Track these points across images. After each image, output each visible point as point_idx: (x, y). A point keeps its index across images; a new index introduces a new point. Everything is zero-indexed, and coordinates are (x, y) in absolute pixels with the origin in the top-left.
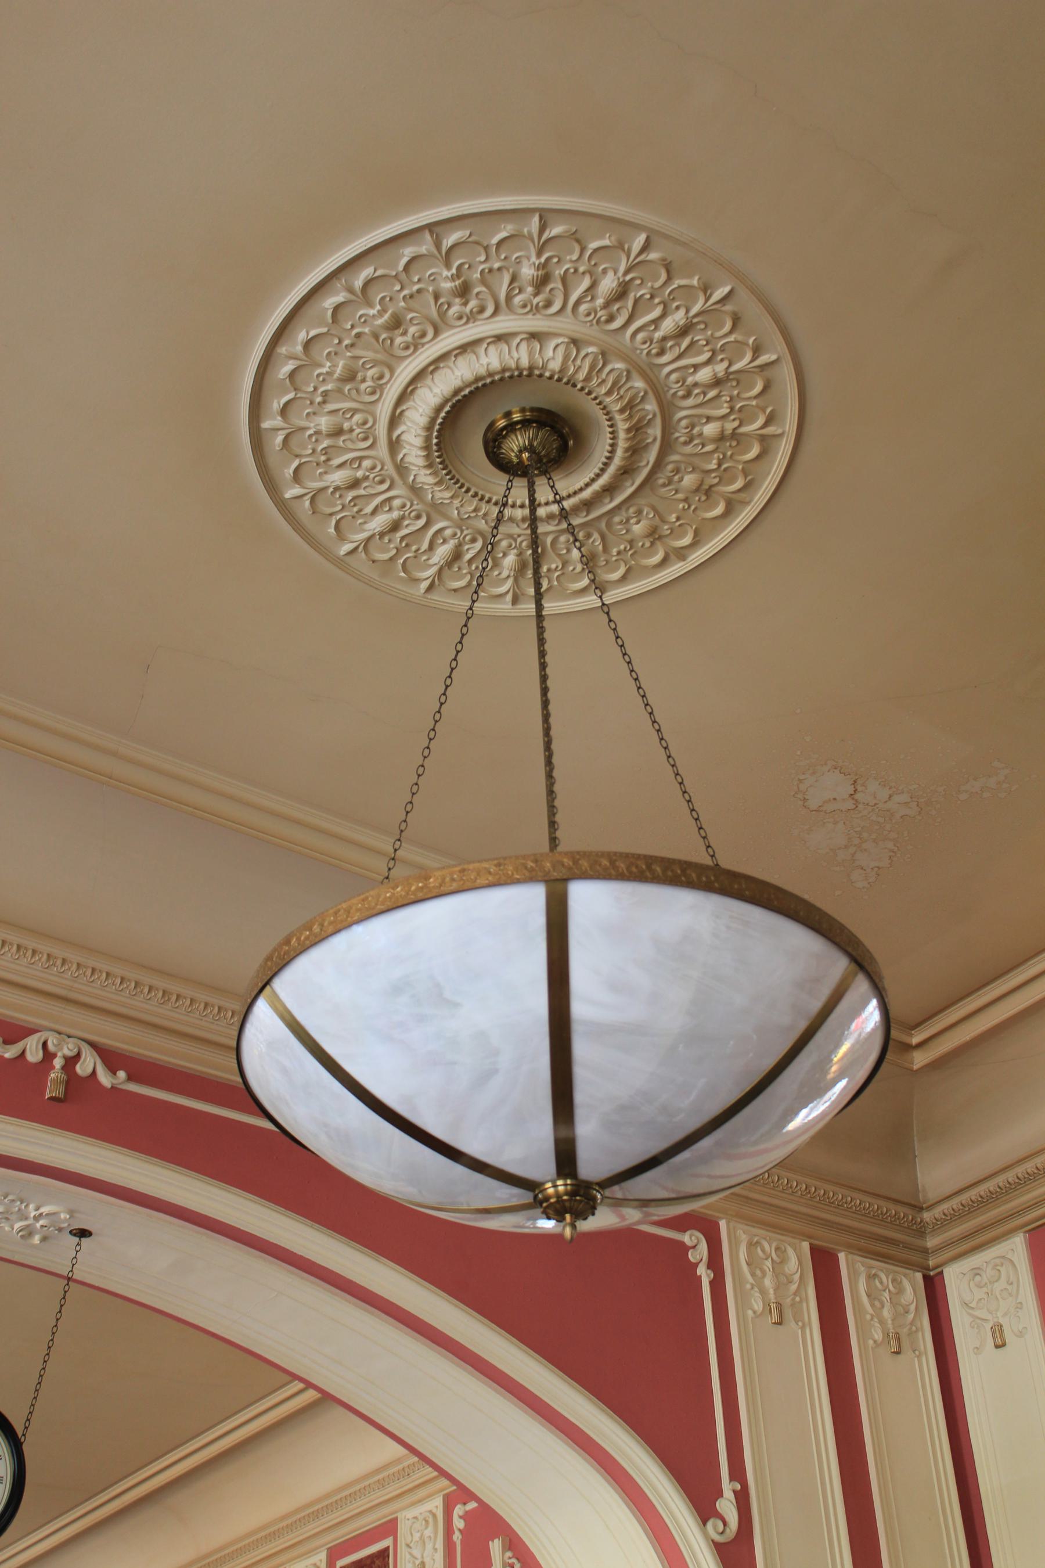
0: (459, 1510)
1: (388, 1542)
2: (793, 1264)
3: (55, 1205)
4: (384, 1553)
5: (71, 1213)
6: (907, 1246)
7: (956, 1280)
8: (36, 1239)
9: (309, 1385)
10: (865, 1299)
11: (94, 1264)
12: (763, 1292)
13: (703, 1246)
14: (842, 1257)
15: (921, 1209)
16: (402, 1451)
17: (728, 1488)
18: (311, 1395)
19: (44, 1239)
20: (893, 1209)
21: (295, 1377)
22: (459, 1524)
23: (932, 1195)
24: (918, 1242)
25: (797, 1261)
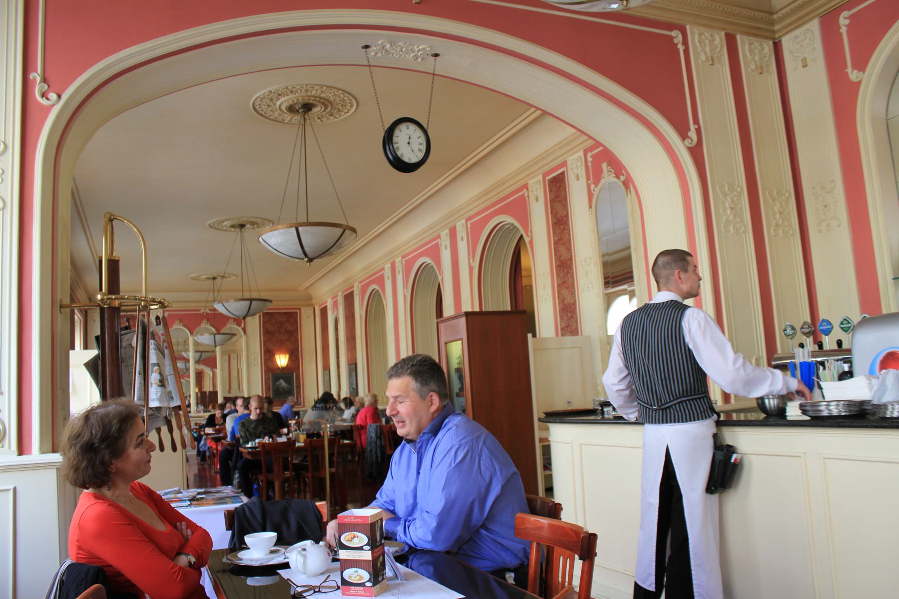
0: (589, 154)
1: (564, 169)
2: (717, 41)
3: (424, 45)
4: (563, 173)
5: (431, 47)
6: (767, 30)
7: (787, 43)
8: (419, 60)
9: (538, 109)
10: (748, 53)
11: (442, 66)
12: (705, 53)
13: (680, 37)
14: (738, 37)
15: (772, 14)
16: (575, 131)
17: (693, 127)
18: (539, 112)
19: (422, 59)
20: (761, 15)
21: (532, 106)
22: (590, 159)
23: (778, 7)
24: (771, 28)
25: (719, 39)
